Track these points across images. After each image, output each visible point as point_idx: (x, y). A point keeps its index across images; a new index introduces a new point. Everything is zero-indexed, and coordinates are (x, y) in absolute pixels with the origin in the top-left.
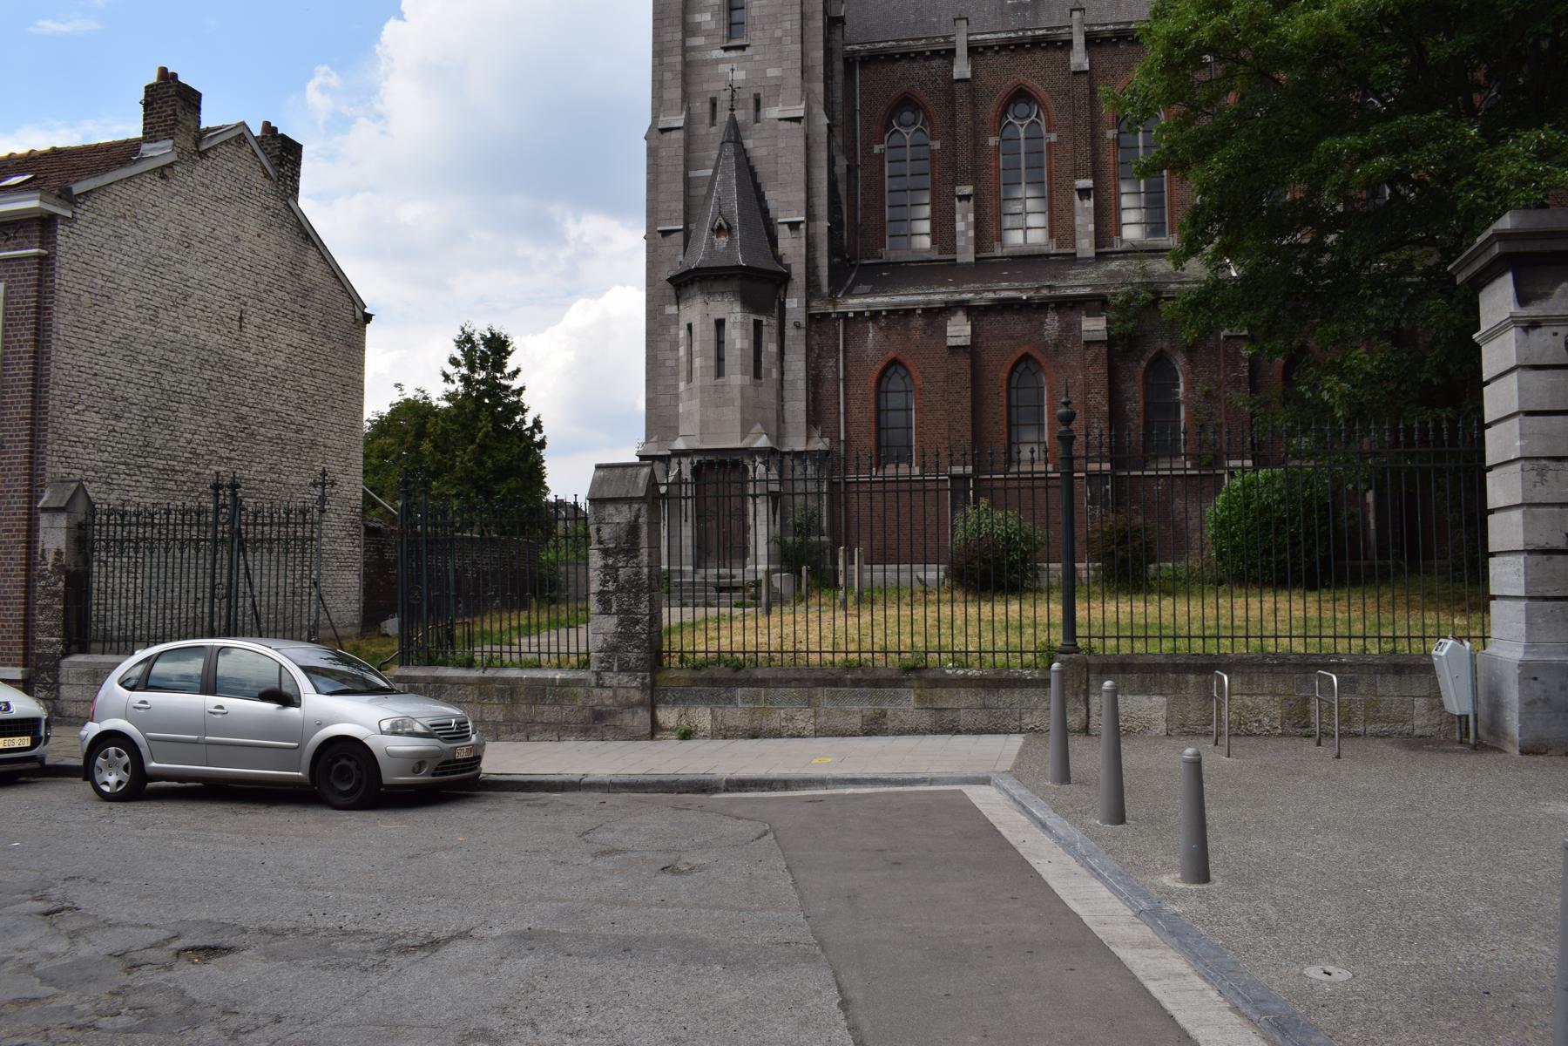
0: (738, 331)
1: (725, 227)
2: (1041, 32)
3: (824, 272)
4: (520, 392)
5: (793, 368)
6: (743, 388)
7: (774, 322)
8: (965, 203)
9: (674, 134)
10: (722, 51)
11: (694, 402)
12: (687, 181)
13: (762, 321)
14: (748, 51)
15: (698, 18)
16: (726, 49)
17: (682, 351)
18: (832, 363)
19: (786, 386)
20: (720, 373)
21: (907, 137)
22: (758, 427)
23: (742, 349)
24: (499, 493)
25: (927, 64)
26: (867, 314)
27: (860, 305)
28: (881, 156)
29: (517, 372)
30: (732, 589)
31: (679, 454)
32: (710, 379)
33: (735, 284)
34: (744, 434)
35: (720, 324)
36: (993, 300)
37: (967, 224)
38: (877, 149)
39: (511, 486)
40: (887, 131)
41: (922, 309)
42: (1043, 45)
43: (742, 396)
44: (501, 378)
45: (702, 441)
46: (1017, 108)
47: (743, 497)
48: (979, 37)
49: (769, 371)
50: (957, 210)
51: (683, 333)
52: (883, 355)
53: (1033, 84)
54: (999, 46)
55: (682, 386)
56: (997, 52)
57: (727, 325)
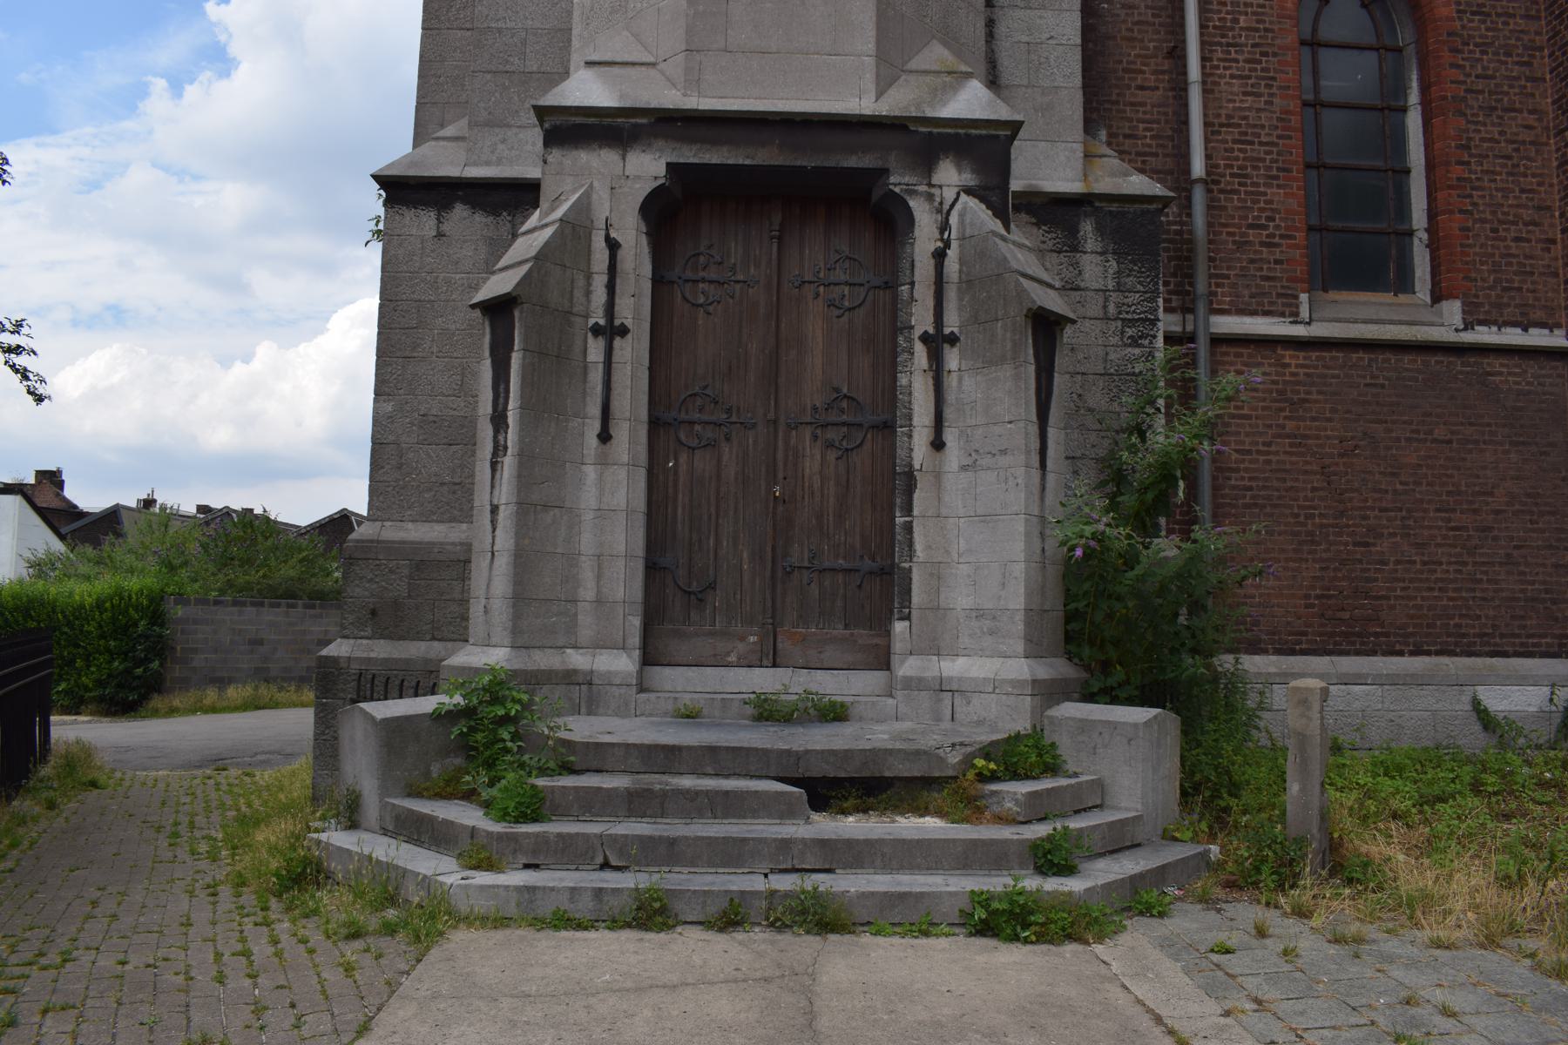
34: (889, 70)
45: (693, 81)
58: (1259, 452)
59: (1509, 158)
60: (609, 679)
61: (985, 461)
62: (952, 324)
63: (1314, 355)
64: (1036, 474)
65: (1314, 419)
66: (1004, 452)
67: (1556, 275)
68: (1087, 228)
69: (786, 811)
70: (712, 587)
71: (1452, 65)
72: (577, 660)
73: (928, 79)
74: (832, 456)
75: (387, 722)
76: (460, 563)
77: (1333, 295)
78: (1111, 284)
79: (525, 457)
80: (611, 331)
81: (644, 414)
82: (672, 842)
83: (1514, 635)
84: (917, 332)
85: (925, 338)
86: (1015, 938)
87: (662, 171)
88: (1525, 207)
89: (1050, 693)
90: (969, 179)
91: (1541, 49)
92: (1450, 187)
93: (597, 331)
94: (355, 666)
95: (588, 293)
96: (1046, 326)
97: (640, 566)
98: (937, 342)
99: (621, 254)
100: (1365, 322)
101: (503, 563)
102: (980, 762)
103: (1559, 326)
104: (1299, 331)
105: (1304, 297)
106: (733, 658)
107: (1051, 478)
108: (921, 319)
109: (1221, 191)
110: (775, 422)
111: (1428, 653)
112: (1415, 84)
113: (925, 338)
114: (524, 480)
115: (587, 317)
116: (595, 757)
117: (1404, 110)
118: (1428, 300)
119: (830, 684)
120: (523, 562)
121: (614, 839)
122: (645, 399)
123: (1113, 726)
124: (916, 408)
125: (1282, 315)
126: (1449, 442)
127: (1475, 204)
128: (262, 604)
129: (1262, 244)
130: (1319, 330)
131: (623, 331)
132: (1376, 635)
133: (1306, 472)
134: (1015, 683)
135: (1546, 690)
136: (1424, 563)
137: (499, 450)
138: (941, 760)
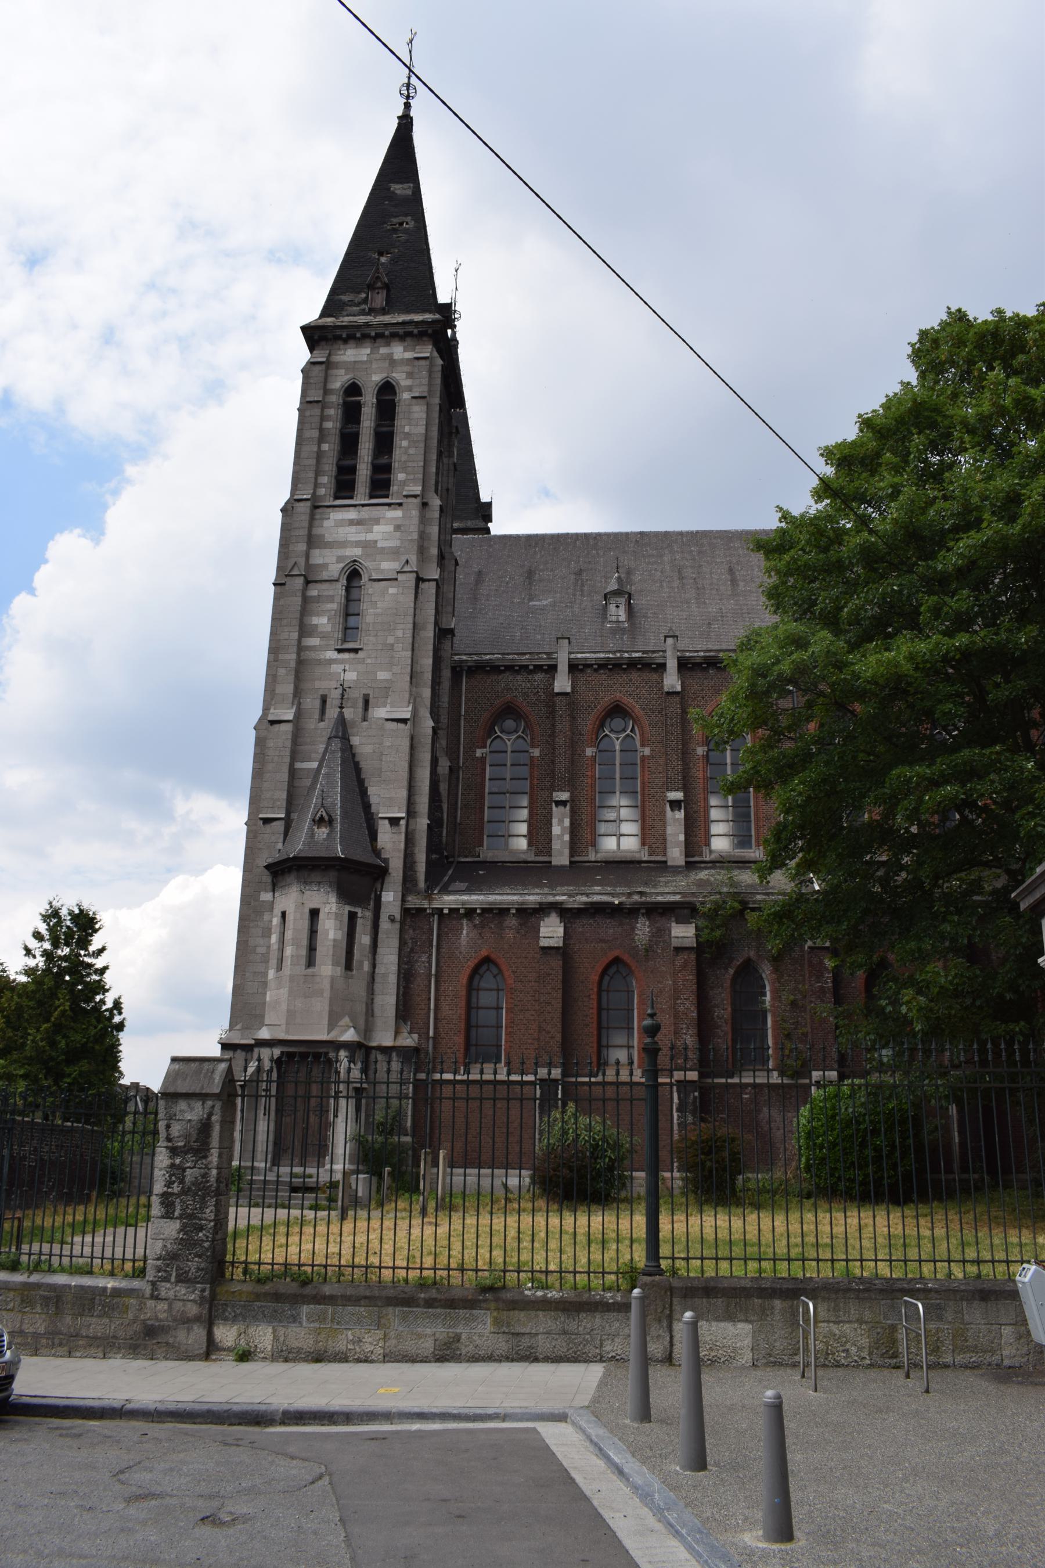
0: (332, 921)
1: (326, 818)
2: (637, 655)
3: (421, 868)
4: (102, 971)
5: (385, 961)
6: (333, 979)
7: (369, 914)
8: (561, 808)
9: (284, 727)
11: (282, 991)
12: (293, 773)
14: (361, 654)
15: (315, 620)
16: (340, 651)
17: (274, 938)
18: (424, 958)
19: (378, 979)
20: (311, 962)
21: (509, 743)
22: (346, 1020)
23: (335, 940)
24: (69, 1075)
25: (530, 677)
26: (462, 911)
27: (456, 902)
28: (483, 759)
30: (306, 1189)
32: (301, 969)
33: (333, 875)
35: (314, 913)
36: (586, 903)
37: (563, 829)
38: (479, 753)
41: (517, 909)
43: (332, 987)
44: (85, 955)
45: (287, 1032)
49: (361, 963)
51: (276, 921)
52: (476, 952)
53: (628, 701)
55: (271, 974)
56: (596, 670)
57: (322, 915)
68: (394, 1054)
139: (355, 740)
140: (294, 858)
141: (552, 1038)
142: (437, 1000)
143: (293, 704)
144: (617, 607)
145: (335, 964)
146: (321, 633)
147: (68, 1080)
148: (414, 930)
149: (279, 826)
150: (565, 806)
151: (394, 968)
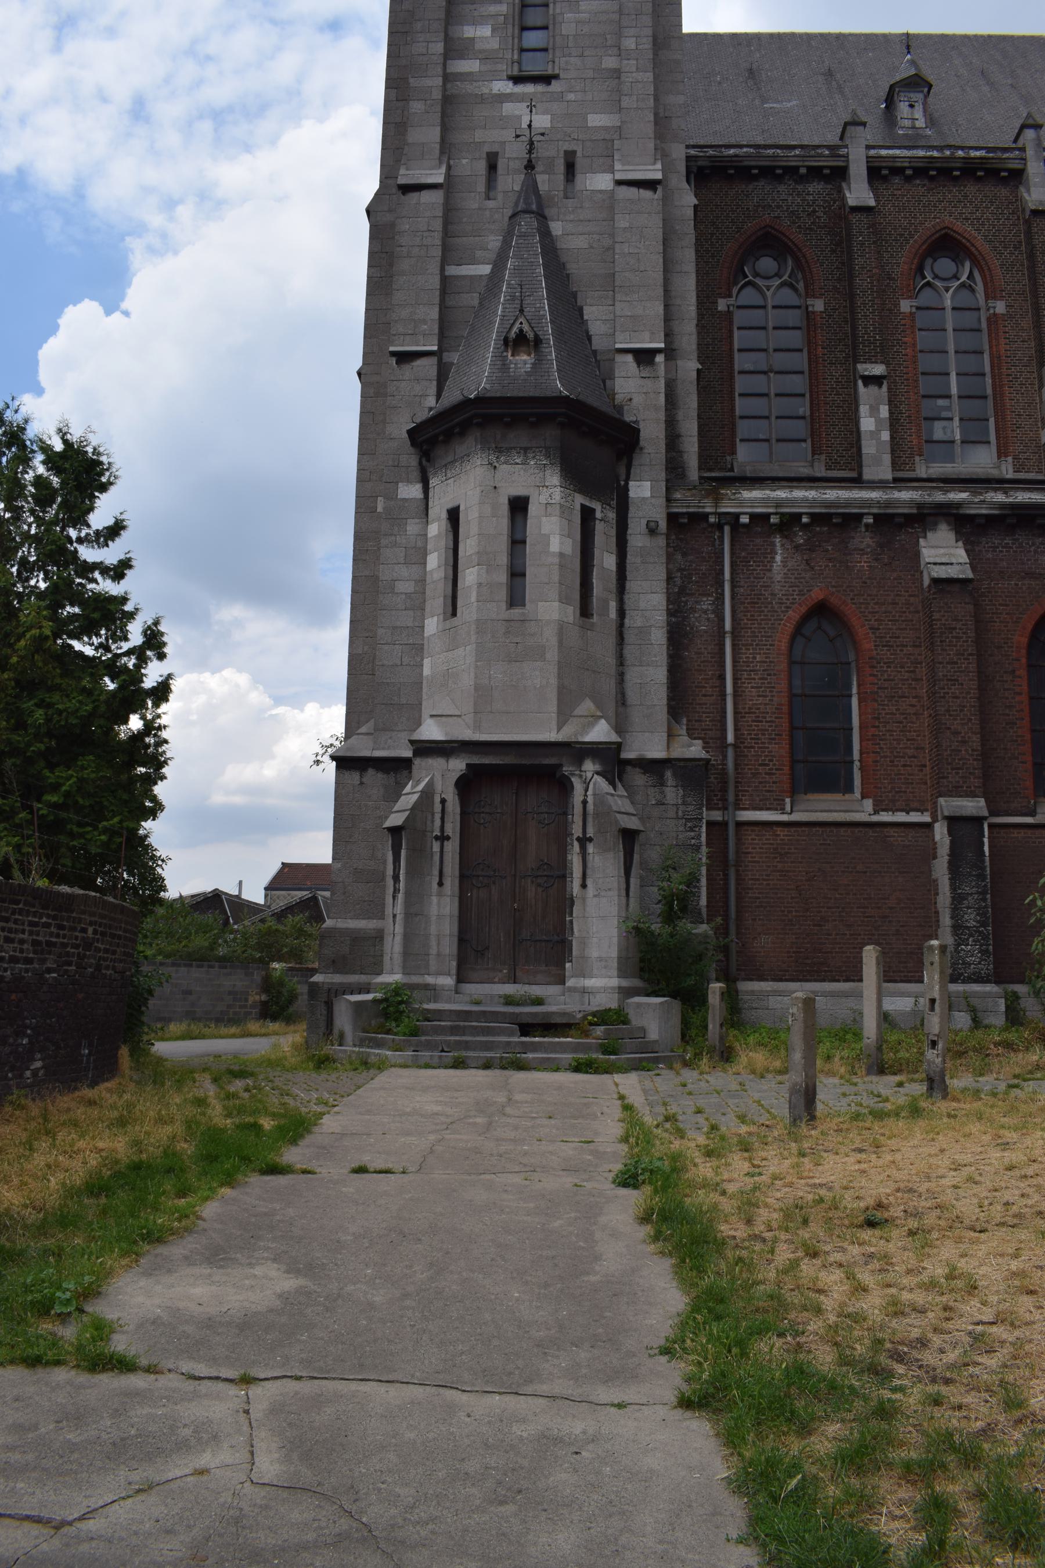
0: (555, 519)
1: (531, 335)
2: (978, 154)
3: (691, 447)
4: (119, 571)
5: (642, 605)
6: (561, 628)
7: (612, 515)
8: (873, 389)
9: (426, 196)
10: (510, 84)
11: (460, 651)
12: (446, 283)
13: (594, 510)
14: (555, 86)
15: (469, 32)
16: (517, 80)
17: (434, 561)
18: (706, 604)
19: (630, 637)
20: (516, 598)
21: (769, 294)
22: (587, 706)
23: (561, 555)
24: (55, 788)
25: (800, 187)
26: (774, 520)
27: (765, 502)
28: (728, 315)
29: (115, 530)
30: (549, 1027)
31: (426, 749)
32: (498, 609)
33: (551, 434)
34: (563, 716)
35: (519, 506)
36: (1003, 506)
37: (879, 421)
38: (722, 305)
39: (85, 774)
40: (736, 283)
41: (876, 516)
42: (980, 174)
43: (560, 642)
44: (80, 540)
45: (477, 727)
46: (936, 264)
47: (561, 838)
48: (884, 152)
49: (606, 608)
50: (861, 401)
51: (436, 528)
52: (801, 593)
53: (966, 229)
54: (914, 169)
55: (432, 625)
56: (908, 179)
57: (533, 509)
58: (764, 880)
59: (901, 722)
60: (443, 988)
61: (602, 894)
62: (590, 833)
63: (793, 830)
64: (624, 900)
65: (792, 862)
66: (610, 890)
67: (926, 783)
68: (668, 774)
69: (511, 1034)
70: (487, 948)
71: (871, 675)
72: (430, 980)
73: (582, 719)
74: (540, 890)
75: (355, 1002)
76: (379, 937)
77: (810, 796)
78: (680, 802)
79: (408, 894)
80: (443, 838)
81: (457, 873)
82: (467, 1042)
83: (900, 971)
84: (575, 837)
85: (578, 839)
86: (587, 1072)
87: (464, 767)
88: (910, 748)
89: (626, 993)
90: (598, 767)
91: (921, 663)
92: (868, 740)
93: (437, 838)
94: (326, 986)
95: (433, 822)
96: (629, 837)
97: (455, 940)
98: (584, 841)
99: (447, 804)
100: (822, 811)
101: (398, 939)
102: (590, 1018)
103: (927, 810)
104: (785, 818)
105: (788, 800)
106: (496, 980)
107: (632, 900)
108: (577, 831)
109: (745, 747)
110: (515, 875)
111: (853, 981)
112: (855, 683)
113: (578, 839)
114: (407, 904)
115: (432, 832)
116: (439, 1015)
117: (850, 696)
118: (859, 797)
119: (536, 990)
120: (407, 938)
121: (446, 1041)
122: (457, 867)
123: (649, 1004)
124: (574, 870)
125: (776, 809)
126: (865, 872)
127: (881, 748)
128: (191, 966)
129: (766, 774)
130: (796, 817)
131: (448, 838)
132: (825, 971)
133: (788, 889)
134: (612, 988)
135: (913, 1000)
136: (851, 935)
137: (396, 891)
138: (574, 1017)
139: (556, 228)
140: (478, 399)
141: (964, 742)
142: (735, 680)
143: (441, 163)
144: (911, 106)
145: (564, 600)
146: (481, 51)
147: (54, 798)
148: (684, 555)
149: (427, 367)
150: (880, 385)
151: (660, 618)
